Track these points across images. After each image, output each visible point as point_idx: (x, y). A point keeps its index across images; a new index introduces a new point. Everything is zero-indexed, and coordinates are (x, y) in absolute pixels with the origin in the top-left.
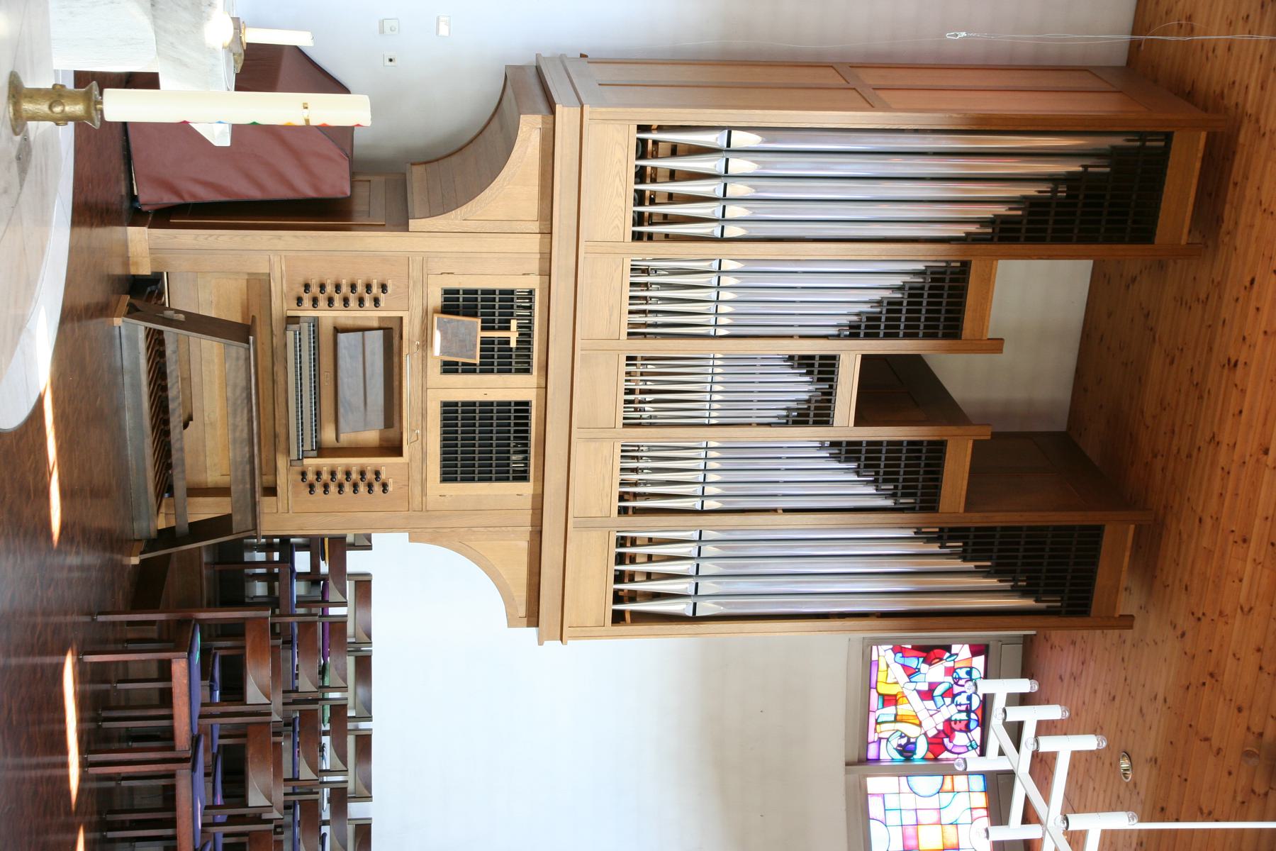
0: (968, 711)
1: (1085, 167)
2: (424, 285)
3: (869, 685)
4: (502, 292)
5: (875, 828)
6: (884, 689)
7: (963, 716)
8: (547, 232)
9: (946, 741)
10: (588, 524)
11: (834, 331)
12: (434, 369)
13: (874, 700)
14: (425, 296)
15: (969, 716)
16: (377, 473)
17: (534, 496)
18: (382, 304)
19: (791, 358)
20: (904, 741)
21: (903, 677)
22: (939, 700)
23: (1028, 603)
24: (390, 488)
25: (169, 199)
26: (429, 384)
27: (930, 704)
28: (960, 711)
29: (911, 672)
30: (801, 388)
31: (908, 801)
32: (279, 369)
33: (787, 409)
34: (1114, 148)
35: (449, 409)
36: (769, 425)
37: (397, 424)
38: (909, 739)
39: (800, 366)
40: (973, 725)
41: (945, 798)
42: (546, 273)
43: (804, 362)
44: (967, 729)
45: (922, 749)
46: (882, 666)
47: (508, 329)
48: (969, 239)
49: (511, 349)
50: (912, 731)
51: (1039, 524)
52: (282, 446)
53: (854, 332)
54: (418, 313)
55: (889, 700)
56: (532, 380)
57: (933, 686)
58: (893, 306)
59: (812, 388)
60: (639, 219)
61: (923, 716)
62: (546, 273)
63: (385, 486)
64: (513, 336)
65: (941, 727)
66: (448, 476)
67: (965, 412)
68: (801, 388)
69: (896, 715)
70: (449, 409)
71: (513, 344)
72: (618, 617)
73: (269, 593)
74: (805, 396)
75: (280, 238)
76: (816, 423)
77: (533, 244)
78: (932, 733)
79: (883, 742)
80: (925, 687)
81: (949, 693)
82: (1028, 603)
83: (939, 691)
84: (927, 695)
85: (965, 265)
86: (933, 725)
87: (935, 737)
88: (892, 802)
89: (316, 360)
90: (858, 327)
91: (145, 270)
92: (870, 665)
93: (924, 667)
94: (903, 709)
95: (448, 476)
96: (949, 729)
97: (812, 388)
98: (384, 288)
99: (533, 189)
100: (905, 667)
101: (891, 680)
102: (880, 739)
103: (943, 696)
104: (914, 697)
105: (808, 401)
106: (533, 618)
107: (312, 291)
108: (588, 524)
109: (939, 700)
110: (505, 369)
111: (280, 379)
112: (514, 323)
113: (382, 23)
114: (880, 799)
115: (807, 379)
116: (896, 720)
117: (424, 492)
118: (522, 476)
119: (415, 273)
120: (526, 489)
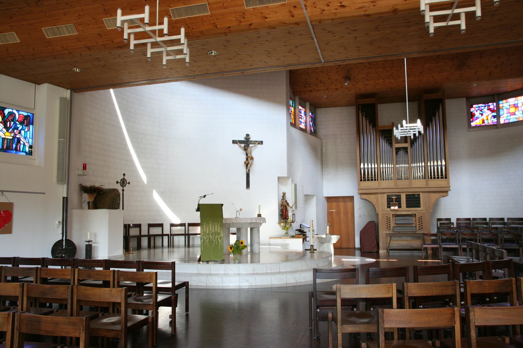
0: (485, 106)
1: (364, 116)
2: (386, 211)
3: (480, 126)
4: (387, 199)
5: (511, 121)
6: (481, 123)
7: (479, 111)
8: (377, 193)
9: (492, 109)
10: (427, 184)
11: (392, 149)
12: (400, 209)
13: (484, 124)
14: (389, 211)
15: (486, 106)
16: (419, 218)
17: (423, 193)
18: (390, 217)
19: (396, 155)
20: (492, 117)
21: (478, 120)
22: (483, 112)
23: (441, 109)
24: (422, 215)
25: (376, 247)
26: (403, 210)
27: (484, 114)
28: (485, 108)
29: (477, 118)
30: (401, 153)
31: (505, 115)
32: (401, 232)
33: (405, 154)
34: (361, 112)
35: (407, 207)
36: (408, 157)
37: (412, 215)
38: (492, 117)
39: (397, 153)
40: (488, 105)
41: (504, 108)
42: (384, 193)
43: (397, 153)
44: (489, 106)
45: (495, 114)
46: (476, 124)
47: (393, 198)
48: (376, 131)
49: (397, 198)
50: (490, 116)
51: (387, 129)
52: (415, 232)
53: (392, 146)
54: (391, 212)
55: (483, 122)
56: (402, 194)
57: (480, 114)
58: (387, 140)
59: (402, 151)
60: (375, 180)
61: (487, 115)
62: (384, 193)
63: (421, 216)
64: (394, 197)
65: (489, 111)
66: (419, 207)
67: (142, 246)
68: (401, 153)
69: (487, 120)
70: (407, 207)
71: (396, 197)
72: (446, 178)
73: (161, 227)
74: (403, 152)
75: (380, 232)
76: (407, 149)
77: (379, 195)
78: (491, 112)
79: (493, 121)
80: (481, 115)
81: (481, 110)
82: (441, 109)
83: (481, 113)
84: (482, 115)
85: (380, 130)
86: (489, 112)
87: (491, 112)
88: (506, 118)
89: (401, 227)
90: (391, 145)
91: (386, 251)
92: (476, 126)
93: (476, 116)
94: (485, 119)
95: (419, 207)
96: (489, 109)
97: (402, 151)
98: (387, 217)
99: (371, 196)
100: (476, 119)
101: (479, 122)
102: (492, 122)
103: (482, 111)
104: (483, 117)
105: (404, 151)
106: (447, 192)
107: (388, 228)
108: (427, 184)
109: (483, 112)
110: (400, 198)
111: (403, 232)
112: (392, 197)
113: (359, 217)
114: (505, 121)
115: (400, 152)
116: (487, 120)
117: (423, 210)
118: (419, 195)
119: (385, 212)
120: (421, 194)
